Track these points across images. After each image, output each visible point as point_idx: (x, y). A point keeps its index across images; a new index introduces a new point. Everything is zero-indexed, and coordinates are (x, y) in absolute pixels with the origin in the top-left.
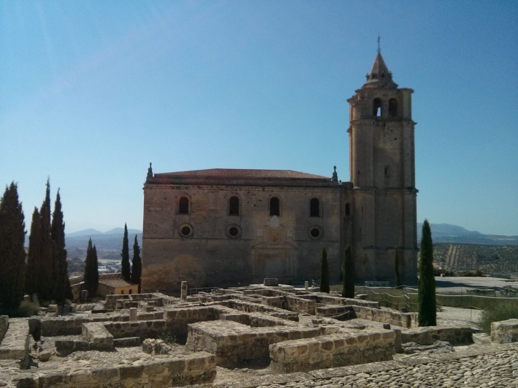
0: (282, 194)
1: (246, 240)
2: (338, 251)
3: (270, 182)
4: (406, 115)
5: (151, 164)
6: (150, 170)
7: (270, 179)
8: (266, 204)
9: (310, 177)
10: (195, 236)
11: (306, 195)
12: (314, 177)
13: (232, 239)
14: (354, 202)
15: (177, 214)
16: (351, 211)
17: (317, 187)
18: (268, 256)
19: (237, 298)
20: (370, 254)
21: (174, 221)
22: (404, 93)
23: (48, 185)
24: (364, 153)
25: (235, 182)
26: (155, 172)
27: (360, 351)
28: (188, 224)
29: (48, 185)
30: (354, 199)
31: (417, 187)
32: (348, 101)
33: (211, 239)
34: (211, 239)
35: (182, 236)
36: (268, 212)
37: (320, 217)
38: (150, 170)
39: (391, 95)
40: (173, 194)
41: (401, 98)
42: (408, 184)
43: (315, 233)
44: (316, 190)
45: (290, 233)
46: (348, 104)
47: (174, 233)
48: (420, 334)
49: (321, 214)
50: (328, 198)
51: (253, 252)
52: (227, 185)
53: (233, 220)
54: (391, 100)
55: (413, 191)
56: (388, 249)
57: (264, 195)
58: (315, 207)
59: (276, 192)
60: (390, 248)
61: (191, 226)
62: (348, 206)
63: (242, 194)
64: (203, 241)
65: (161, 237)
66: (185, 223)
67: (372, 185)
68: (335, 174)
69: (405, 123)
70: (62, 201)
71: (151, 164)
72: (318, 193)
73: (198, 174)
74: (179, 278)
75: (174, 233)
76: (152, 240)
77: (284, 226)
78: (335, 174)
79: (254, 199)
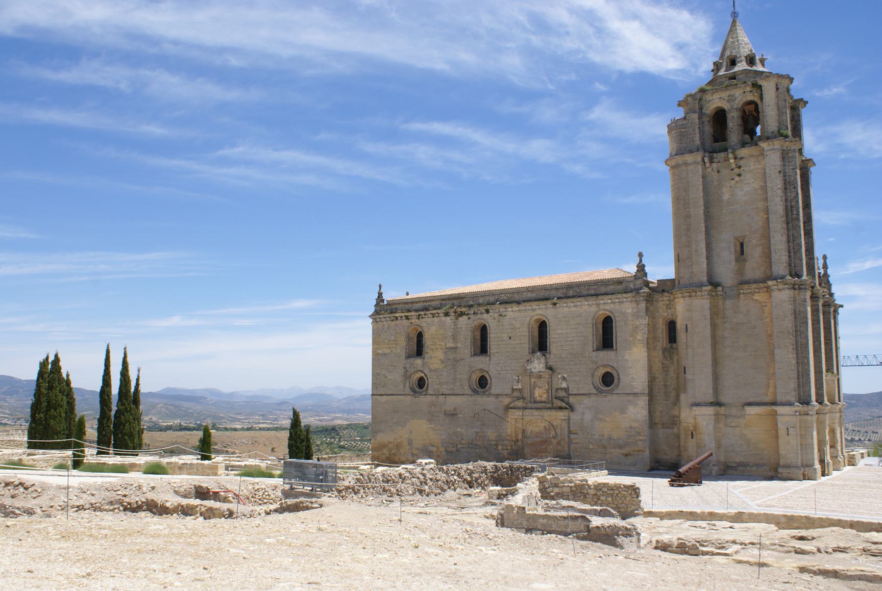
6: (380, 294)
10: (430, 392)
11: (589, 310)
15: (409, 356)
19: (774, 506)
21: (405, 368)
23: (108, 352)
24: (698, 219)
26: (388, 297)
28: (422, 372)
29: (108, 352)
33: (449, 395)
34: (449, 395)
35: (414, 392)
38: (380, 294)
40: (403, 326)
44: (607, 299)
48: (138, 408)
49: (612, 347)
50: (626, 311)
53: (480, 362)
59: (542, 311)
63: (489, 319)
64: (441, 398)
65: (390, 392)
67: (705, 279)
68: (641, 268)
70: (129, 359)
74: (413, 455)
78: (641, 268)
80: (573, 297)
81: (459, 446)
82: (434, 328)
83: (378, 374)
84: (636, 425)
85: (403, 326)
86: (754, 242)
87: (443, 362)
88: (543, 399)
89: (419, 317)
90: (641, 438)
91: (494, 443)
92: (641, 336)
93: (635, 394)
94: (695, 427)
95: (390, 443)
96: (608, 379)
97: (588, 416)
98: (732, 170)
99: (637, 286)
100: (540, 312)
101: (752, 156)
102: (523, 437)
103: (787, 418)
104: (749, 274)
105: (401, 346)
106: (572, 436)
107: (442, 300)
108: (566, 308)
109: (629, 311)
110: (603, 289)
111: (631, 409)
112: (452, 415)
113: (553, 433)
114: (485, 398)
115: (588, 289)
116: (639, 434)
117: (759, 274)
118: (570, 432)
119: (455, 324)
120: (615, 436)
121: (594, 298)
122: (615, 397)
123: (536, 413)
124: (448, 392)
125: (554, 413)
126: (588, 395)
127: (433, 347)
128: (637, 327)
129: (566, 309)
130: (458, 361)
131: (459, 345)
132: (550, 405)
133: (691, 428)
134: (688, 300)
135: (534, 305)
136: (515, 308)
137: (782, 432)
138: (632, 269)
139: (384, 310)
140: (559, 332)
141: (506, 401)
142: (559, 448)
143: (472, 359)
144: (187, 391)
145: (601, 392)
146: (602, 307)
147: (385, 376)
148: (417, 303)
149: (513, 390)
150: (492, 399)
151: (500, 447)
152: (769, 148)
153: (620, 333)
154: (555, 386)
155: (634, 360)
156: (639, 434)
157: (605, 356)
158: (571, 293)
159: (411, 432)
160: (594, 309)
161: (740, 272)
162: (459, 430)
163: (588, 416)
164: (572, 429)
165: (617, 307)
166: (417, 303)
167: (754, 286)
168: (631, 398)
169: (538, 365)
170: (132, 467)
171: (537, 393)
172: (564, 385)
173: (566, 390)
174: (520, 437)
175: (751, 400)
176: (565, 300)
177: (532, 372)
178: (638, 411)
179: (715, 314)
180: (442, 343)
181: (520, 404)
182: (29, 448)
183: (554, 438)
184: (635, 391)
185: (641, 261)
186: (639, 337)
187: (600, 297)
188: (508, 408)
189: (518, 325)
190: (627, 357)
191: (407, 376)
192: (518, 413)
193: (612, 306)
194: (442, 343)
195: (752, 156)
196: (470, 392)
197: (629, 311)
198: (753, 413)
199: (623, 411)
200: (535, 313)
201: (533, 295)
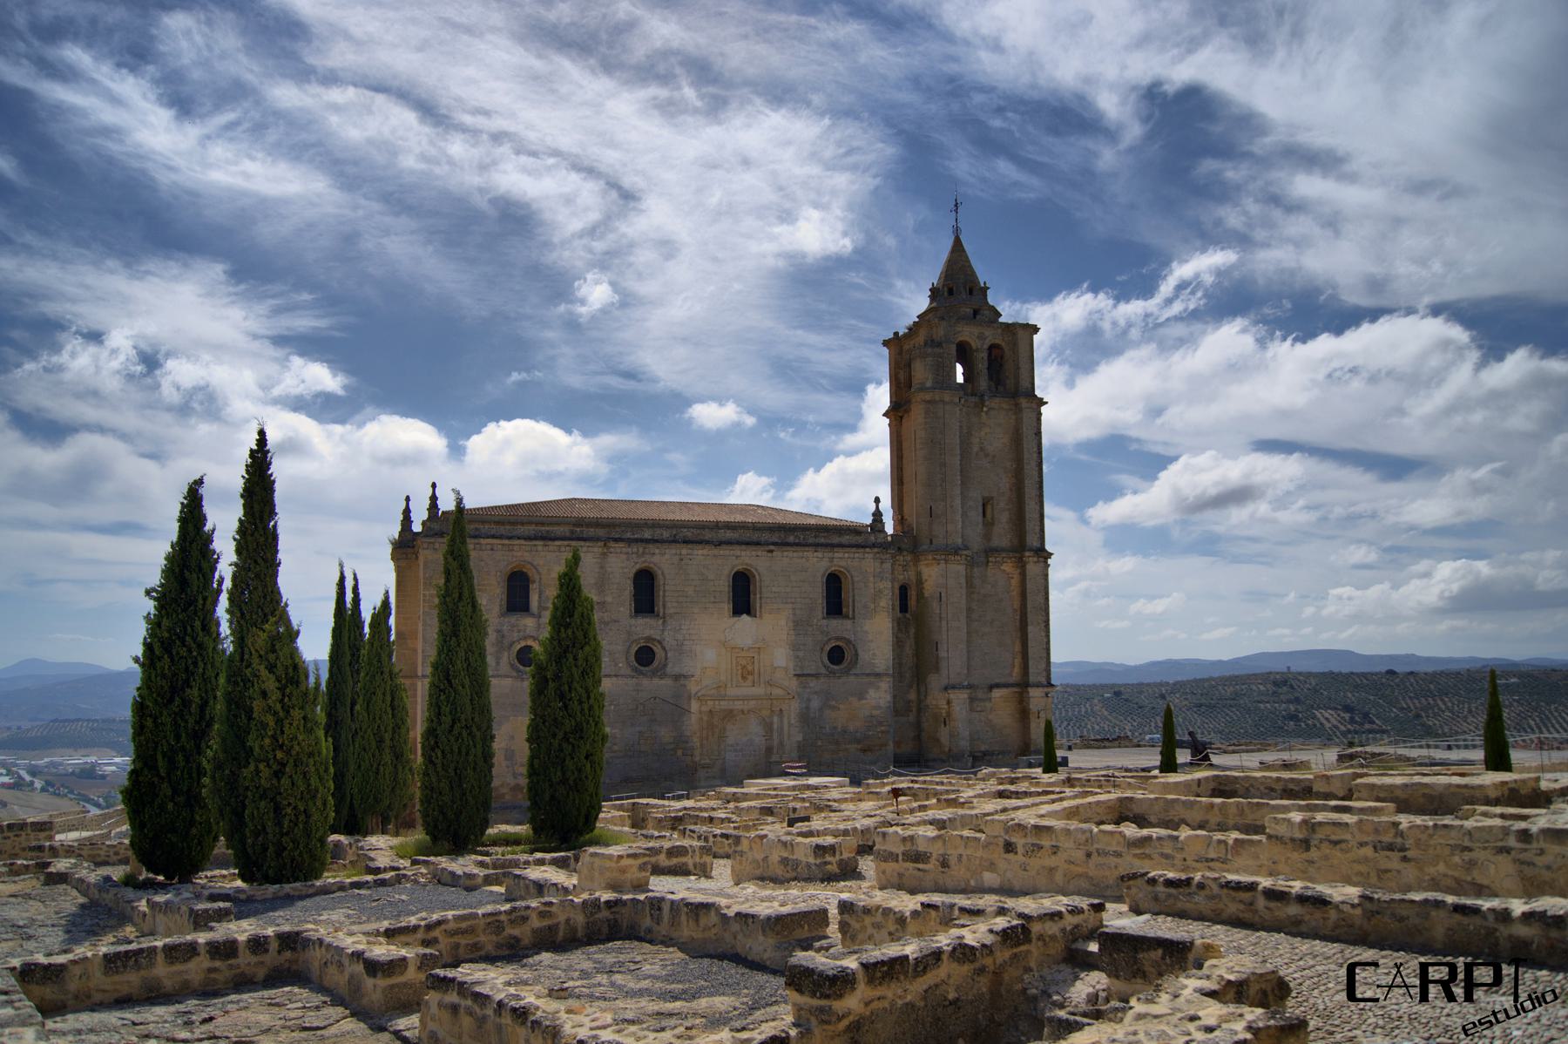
0: (663, 561)
1: (677, 677)
2: (889, 697)
3: (729, 535)
4: (1024, 384)
5: (434, 486)
7: (729, 526)
8: (724, 586)
9: (779, 519)
11: (818, 563)
12: (829, 522)
13: (641, 673)
14: (920, 582)
15: (503, 615)
16: (912, 602)
17: (841, 546)
18: (729, 715)
20: (959, 698)
22: (1021, 333)
25: (647, 535)
27: (1353, 906)
30: (919, 574)
31: (1048, 548)
32: (886, 343)
35: (636, 670)
36: (727, 607)
37: (847, 617)
38: (434, 498)
39: (991, 336)
41: (1014, 345)
42: (1032, 541)
43: (836, 655)
44: (839, 554)
45: (781, 657)
46: (886, 351)
49: (659, 608)
51: (694, 706)
52: (630, 541)
53: (645, 627)
54: (992, 347)
55: (1043, 555)
56: (991, 687)
57: (719, 566)
58: (835, 596)
60: (998, 686)
62: (904, 591)
63: (663, 561)
66: (525, 638)
67: (960, 541)
68: (460, 501)
69: (1023, 402)
71: (434, 486)
72: (842, 560)
73: (544, 512)
77: (772, 639)
79: (692, 576)
84: (876, 712)
86: (1002, 505)
93: (878, 675)
94: (949, 714)
100: (747, 561)
108: (786, 559)
110: (708, 535)
111: (872, 693)
114: (656, 681)
116: (880, 723)
120: (851, 729)
122: (852, 678)
126: (816, 676)
128: (880, 591)
130: (606, 624)
131: (609, 599)
135: (737, 550)
143: (633, 621)
144: (1128, 670)
150: (668, 682)
151: (680, 753)
156: (880, 723)
157: (837, 626)
159: (512, 738)
161: (987, 536)
168: (872, 679)
178: (880, 696)
182: (1308, 762)
186: (883, 603)
190: (866, 628)
196: (629, 672)
199: (861, 696)
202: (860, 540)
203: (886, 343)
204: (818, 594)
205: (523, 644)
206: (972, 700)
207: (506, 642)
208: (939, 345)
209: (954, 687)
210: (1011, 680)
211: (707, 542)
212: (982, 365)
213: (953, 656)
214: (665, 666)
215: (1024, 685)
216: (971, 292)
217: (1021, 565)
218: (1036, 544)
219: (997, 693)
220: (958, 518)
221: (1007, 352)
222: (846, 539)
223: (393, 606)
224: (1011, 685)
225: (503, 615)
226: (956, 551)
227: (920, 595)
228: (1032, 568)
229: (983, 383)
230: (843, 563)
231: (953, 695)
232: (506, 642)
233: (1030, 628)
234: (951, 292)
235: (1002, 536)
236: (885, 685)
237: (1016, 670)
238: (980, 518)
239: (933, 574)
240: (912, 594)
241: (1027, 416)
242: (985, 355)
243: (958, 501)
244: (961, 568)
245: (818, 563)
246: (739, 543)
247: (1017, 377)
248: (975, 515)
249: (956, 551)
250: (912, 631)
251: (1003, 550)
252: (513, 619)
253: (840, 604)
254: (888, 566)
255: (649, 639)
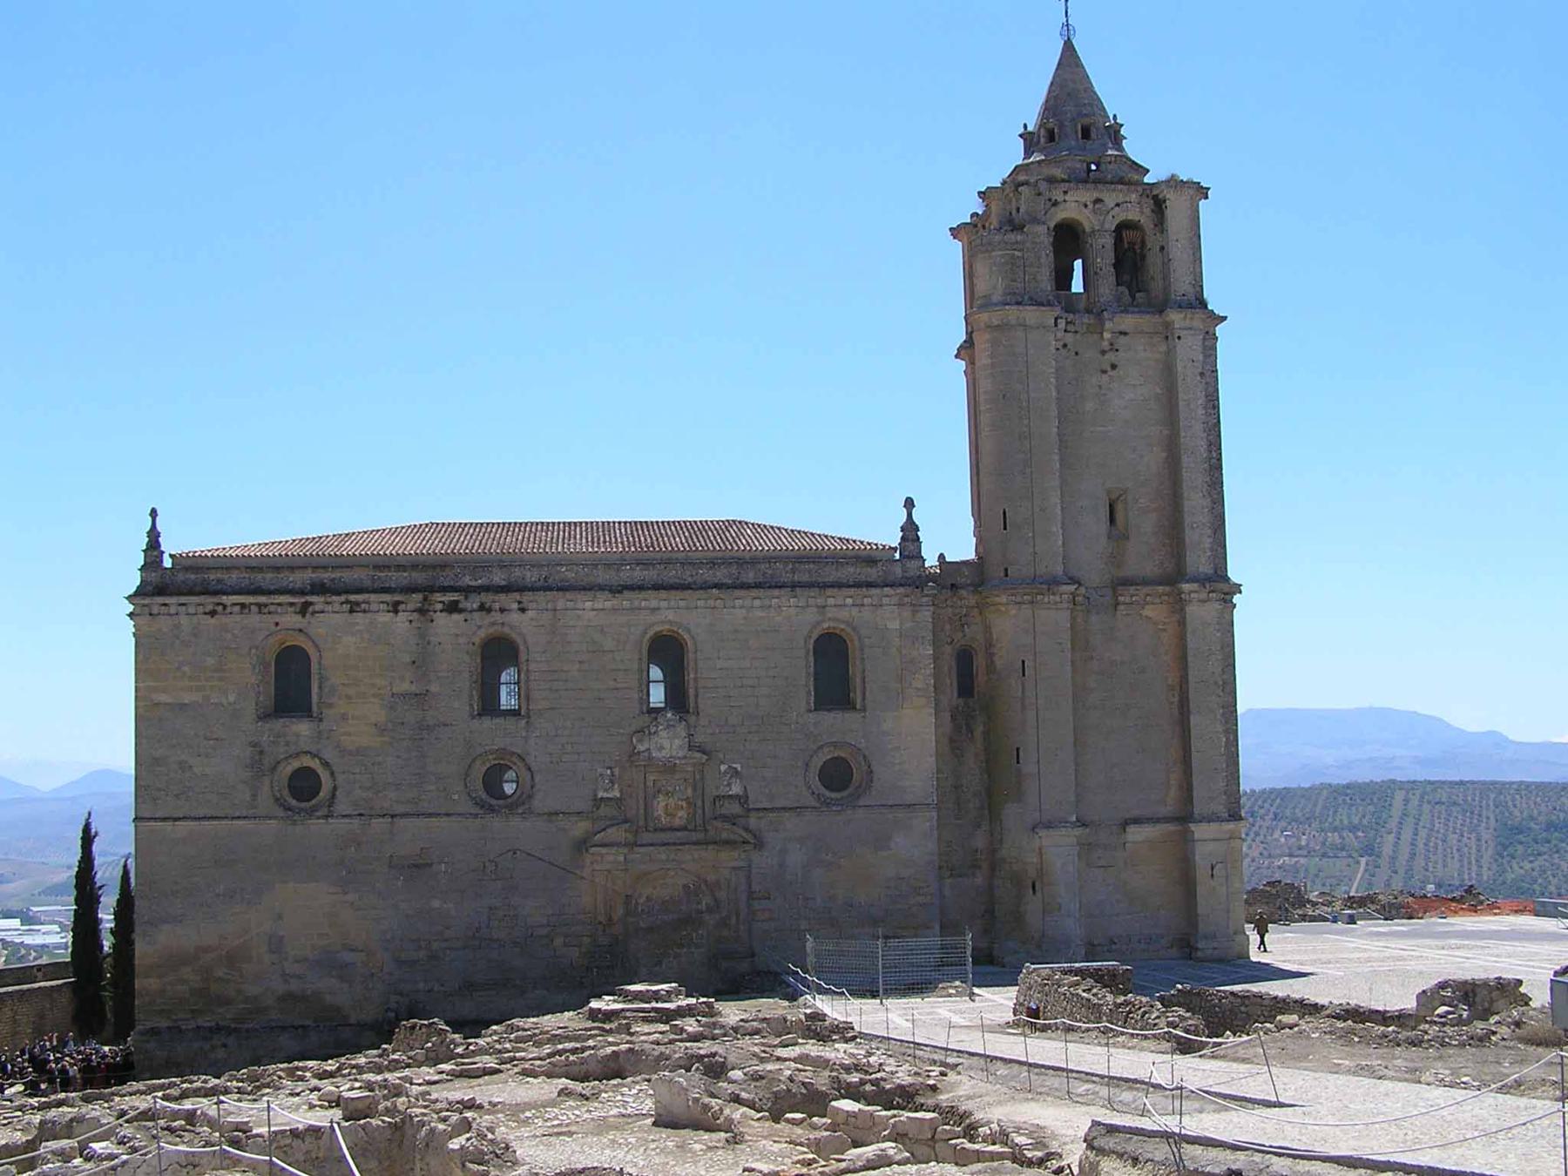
6: (154, 535)
11: (798, 617)
15: (264, 717)
17: (839, 585)
31: (1234, 574)
32: (955, 232)
38: (154, 535)
42: (1198, 562)
44: (833, 598)
47: (254, 796)
55: (1223, 589)
56: (1125, 823)
60: (1137, 821)
61: (326, 764)
62: (965, 659)
63: (525, 622)
68: (910, 531)
72: (841, 610)
75: (254, 796)
76: (168, 825)
78: (910, 531)
80: (758, 586)
81: (435, 946)
82: (340, 638)
83: (157, 761)
85: (264, 627)
87: (382, 730)
88: (677, 822)
89: (304, 610)
90: (920, 899)
91: (545, 931)
92: (923, 679)
94: (1041, 872)
95: (206, 950)
96: (839, 776)
97: (796, 858)
98: (1103, 352)
99: (895, 570)
100: (671, 616)
101: (1142, 332)
102: (627, 913)
103: (1211, 846)
104: (1132, 568)
105: (247, 681)
106: (756, 905)
107: (377, 567)
108: (742, 611)
109: (894, 625)
112: (417, 867)
113: (706, 901)
114: (516, 822)
115: (793, 571)
117: (1150, 569)
118: (751, 895)
119: (422, 635)
121: (814, 592)
123: (662, 854)
124: (400, 809)
125: (709, 853)
127: (351, 691)
129: (740, 613)
131: (434, 688)
132: (700, 836)
133: (1032, 873)
134: (1026, 611)
135: (652, 599)
136: (604, 601)
137: (1202, 873)
138: (892, 537)
139: (172, 588)
140: (720, 664)
141: (580, 828)
142: (725, 933)
143: (476, 723)
145: (827, 803)
146: (831, 612)
147: (184, 766)
148: (292, 569)
149: (598, 802)
151: (558, 941)
152: (1183, 324)
153: (872, 670)
154: (711, 791)
155: (907, 735)
157: (834, 722)
158: (750, 576)
160: (811, 616)
162: (436, 904)
163: (796, 858)
164: (756, 887)
165: (867, 614)
166: (292, 569)
167: (1147, 590)
169: (668, 743)
170: (1123, 1034)
171: (660, 805)
172: (736, 789)
173: (742, 799)
174: (620, 911)
175: (1136, 813)
176: (738, 593)
177: (650, 758)
179: (1080, 642)
180: (379, 682)
181: (615, 834)
183: (710, 910)
184: (909, 799)
185: (910, 515)
187: (829, 592)
188: (582, 845)
189: (609, 644)
191: (259, 764)
192: (614, 856)
193: (855, 611)
194: (379, 682)
195: (1142, 332)
197: (894, 625)
198: (1139, 838)
200: (653, 619)
201: (650, 575)
202: (873, 573)
203: (955, 232)
204: (801, 670)
205: (296, 764)
206: (1086, 848)
207: (267, 761)
208: (1018, 227)
209: (1049, 826)
210: (1165, 811)
211: (601, 588)
212: (1105, 260)
213: (1048, 773)
214: (530, 797)
215: (1185, 817)
216: (1086, 133)
217: (1178, 605)
218: (1206, 568)
219: (1136, 834)
220: (1056, 528)
221: (1153, 241)
222: (849, 573)
223: (1255, 988)
224: (1167, 820)
225: (264, 717)
226: (1052, 583)
227: (991, 667)
228: (1200, 612)
229: (1107, 287)
230: (844, 614)
231: (1047, 838)
232: (267, 761)
233: (1193, 720)
234: (1051, 137)
235: (1143, 557)
236: (924, 822)
237: (1173, 793)
238: (1104, 525)
239: (1009, 624)
240: (979, 662)
241: (1188, 348)
242: (1108, 241)
243: (1055, 499)
244: (1063, 617)
245: (798, 617)
246: (657, 587)
247: (1166, 277)
248: (1096, 524)
249: (1052, 583)
250: (979, 730)
251: (1145, 582)
252: (278, 725)
253: (845, 680)
254: (926, 615)
255: (502, 752)
